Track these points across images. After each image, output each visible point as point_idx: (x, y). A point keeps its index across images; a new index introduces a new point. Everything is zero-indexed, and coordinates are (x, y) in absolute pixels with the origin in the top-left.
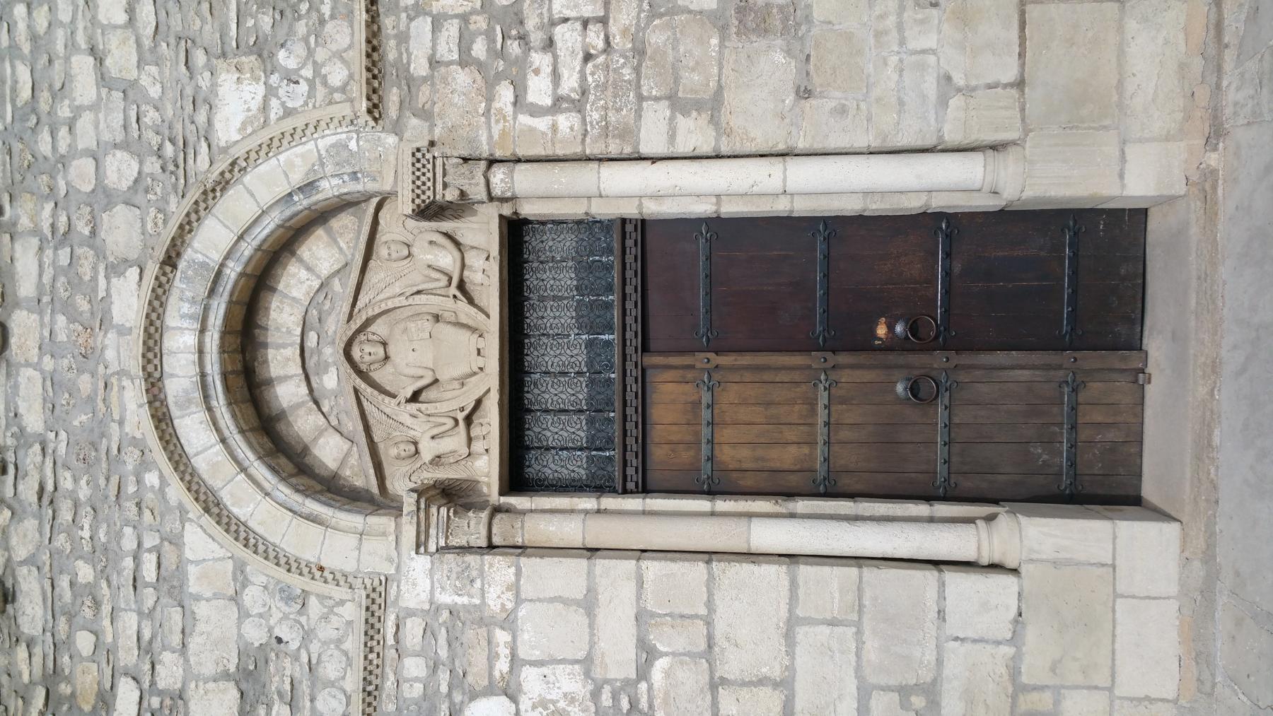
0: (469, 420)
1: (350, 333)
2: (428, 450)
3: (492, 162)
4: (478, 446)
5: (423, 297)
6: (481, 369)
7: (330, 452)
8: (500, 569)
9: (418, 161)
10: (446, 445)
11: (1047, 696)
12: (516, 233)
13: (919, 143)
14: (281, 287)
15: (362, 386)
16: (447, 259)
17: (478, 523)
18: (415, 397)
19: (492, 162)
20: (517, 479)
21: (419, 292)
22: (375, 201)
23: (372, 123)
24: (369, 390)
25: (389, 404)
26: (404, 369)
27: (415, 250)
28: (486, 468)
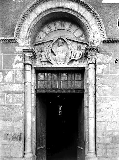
0: (48, 62)
1: (64, 39)
2: (43, 54)
3: (95, 64)
4: (43, 63)
5: (71, 53)
6: (57, 64)
7: (42, 35)
8: (21, 65)
9: (96, 50)
10: (44, 57)
11: (74, 79)
12: (81, 71)
13: (97, 129)
14: (73, 26)
15: (54, 41)
16: (77, 57)
17: (28, 46)
18: (52, 51)
19: (95, 64)
20: (38, 71)
21: (71, 52)
22: (88, 43)
23: (103, 41)
24: (53, 43)
25: (51, 46)
26: (56, 49)
27: (79, 51)
28: (39, 64)
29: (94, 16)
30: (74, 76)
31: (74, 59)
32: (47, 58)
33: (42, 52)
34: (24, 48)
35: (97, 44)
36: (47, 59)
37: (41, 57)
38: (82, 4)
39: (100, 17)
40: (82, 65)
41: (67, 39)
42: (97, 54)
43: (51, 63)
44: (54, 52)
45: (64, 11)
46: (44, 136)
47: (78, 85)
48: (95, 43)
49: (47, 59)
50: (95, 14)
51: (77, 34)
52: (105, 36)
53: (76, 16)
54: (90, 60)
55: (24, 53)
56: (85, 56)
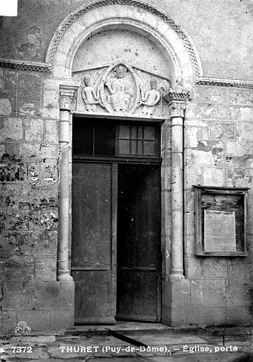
3: (184, 119)
4: (89, 107)
12: (156, 126)
15: (109, 69)
16: (151, 102)
29: (183, 39)
30: (143, 131)
31: (146, 103)
32: (97, 98)
33: (86, 86)
34: (62, 83)
35: (188, 86)
36: (96, 100)
37: (84, 95)
38: (147, 8)
39: (196, 51)
40: (157, 115)
41: (134, 68)
42: (187, 102)
43: (104, 108)
44: (110, 87)
45: (133, 24)
46: (13, 82)
47: (148, 151)
48: (184, 84)
49: (96, 100)
50: (185, 37)
51: (145, 58)
52: (201, 74)
53: (153, 34)
54: (176, 110)
55: (62, 90)
56: (167, 100)
